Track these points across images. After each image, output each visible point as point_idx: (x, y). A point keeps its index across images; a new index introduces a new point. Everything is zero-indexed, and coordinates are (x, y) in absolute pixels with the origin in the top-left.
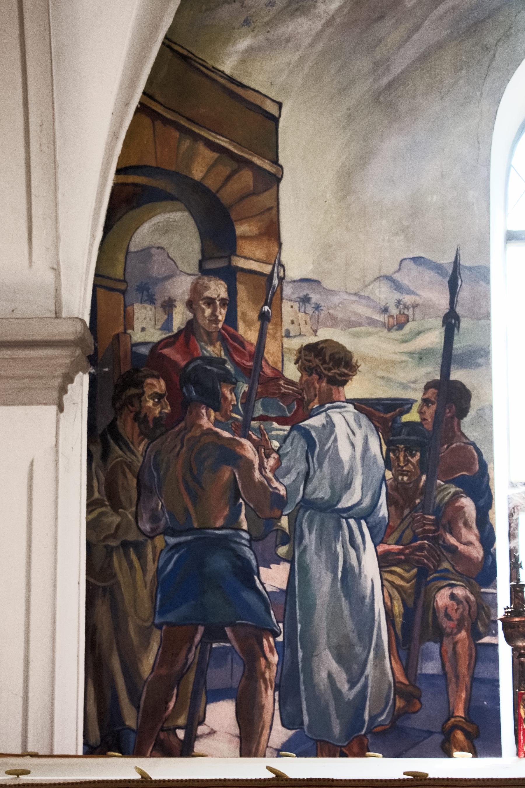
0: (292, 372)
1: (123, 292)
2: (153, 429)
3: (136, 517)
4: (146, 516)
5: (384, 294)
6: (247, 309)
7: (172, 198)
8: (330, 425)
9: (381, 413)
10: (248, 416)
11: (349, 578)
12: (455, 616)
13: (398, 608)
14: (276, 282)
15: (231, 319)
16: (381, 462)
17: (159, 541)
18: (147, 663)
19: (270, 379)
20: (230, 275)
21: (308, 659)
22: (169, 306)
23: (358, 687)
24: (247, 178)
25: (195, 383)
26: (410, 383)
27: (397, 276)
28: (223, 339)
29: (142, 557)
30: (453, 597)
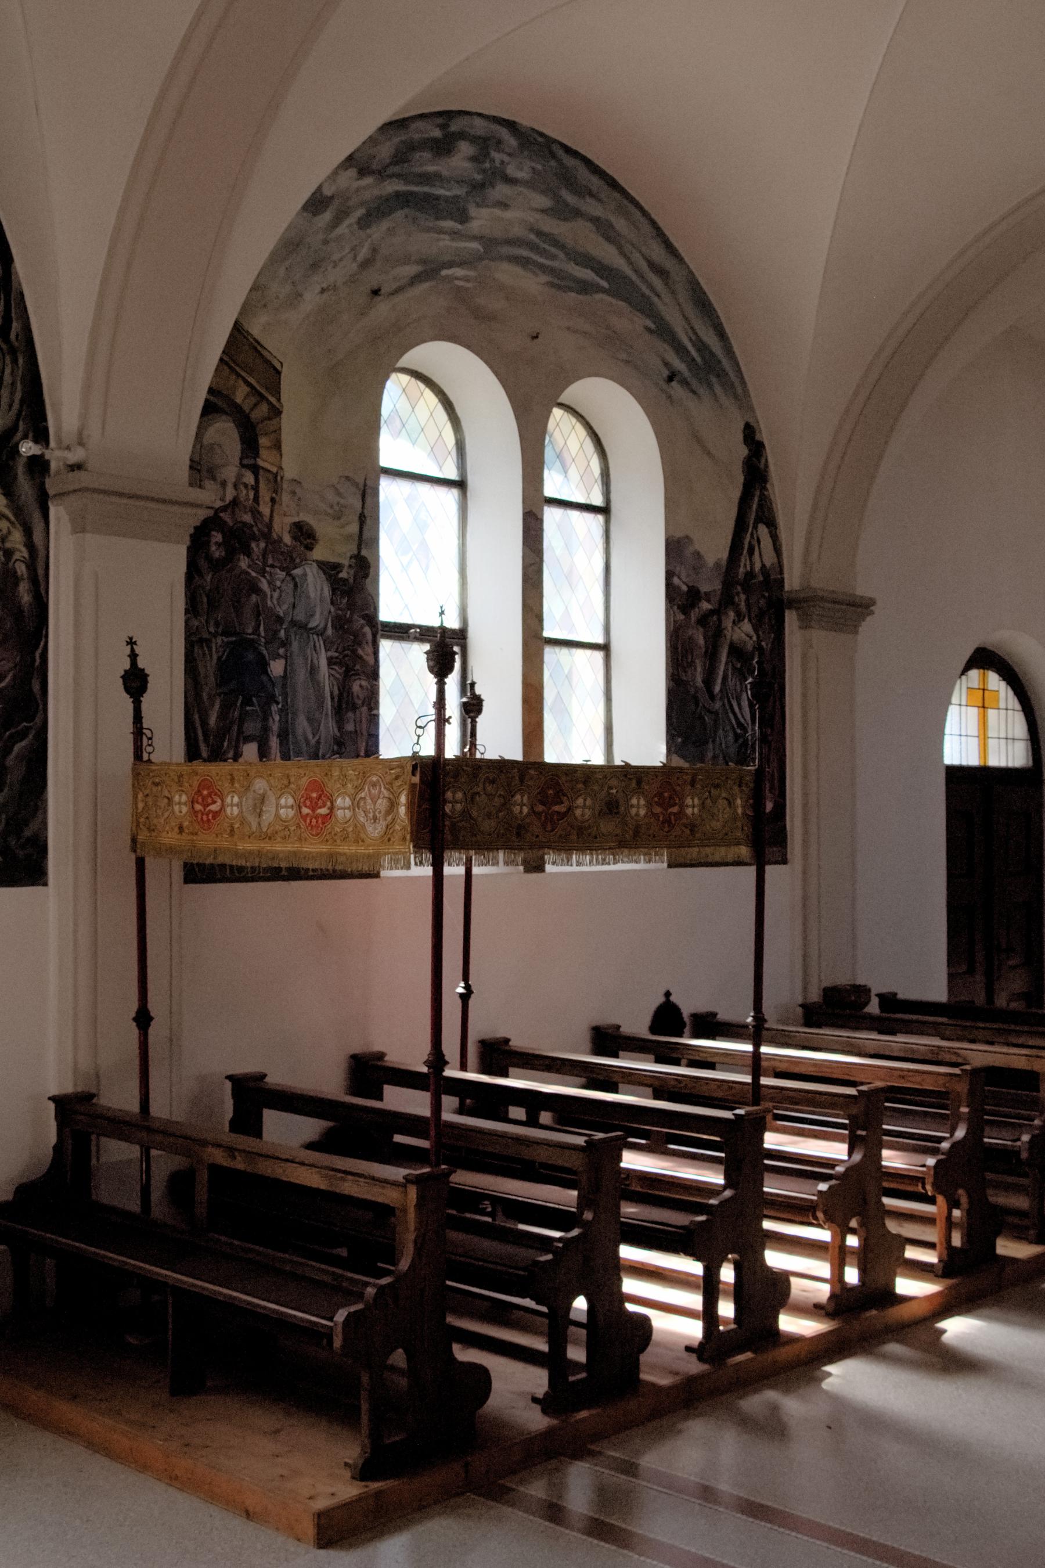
0: (287, 539)
1: (199, 471)
2: (217, 566)
3: (207, 622)
4: (212, 623)
5: (330, 496)
6: (265, 494)
7: (226, 413)
8: (305, 575)
9: (330, 569)
10: (265, 564)
11: (313, 670)
12: (361, 696)
13: (336, 692)
14: (279, 478)
15: (256, 499)
16: (329, 601)
17: (219, 640)
18: (213, 720)
19: (275, 541)
20: (255, 469)
21: (293, 719)
22: (224, 484)
23: (317, 737)
24: (264, 408)
25: (239, 540)
26: (342, 554)
27: (338, 486)
28: (251, 511)
29: (210, 649)
30: (361, 686)
